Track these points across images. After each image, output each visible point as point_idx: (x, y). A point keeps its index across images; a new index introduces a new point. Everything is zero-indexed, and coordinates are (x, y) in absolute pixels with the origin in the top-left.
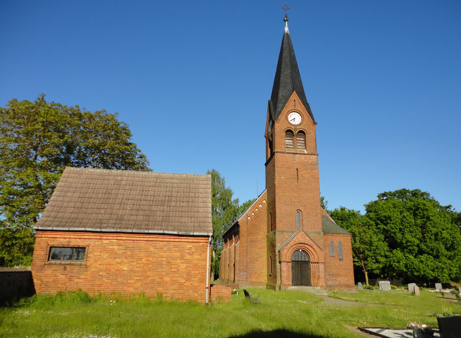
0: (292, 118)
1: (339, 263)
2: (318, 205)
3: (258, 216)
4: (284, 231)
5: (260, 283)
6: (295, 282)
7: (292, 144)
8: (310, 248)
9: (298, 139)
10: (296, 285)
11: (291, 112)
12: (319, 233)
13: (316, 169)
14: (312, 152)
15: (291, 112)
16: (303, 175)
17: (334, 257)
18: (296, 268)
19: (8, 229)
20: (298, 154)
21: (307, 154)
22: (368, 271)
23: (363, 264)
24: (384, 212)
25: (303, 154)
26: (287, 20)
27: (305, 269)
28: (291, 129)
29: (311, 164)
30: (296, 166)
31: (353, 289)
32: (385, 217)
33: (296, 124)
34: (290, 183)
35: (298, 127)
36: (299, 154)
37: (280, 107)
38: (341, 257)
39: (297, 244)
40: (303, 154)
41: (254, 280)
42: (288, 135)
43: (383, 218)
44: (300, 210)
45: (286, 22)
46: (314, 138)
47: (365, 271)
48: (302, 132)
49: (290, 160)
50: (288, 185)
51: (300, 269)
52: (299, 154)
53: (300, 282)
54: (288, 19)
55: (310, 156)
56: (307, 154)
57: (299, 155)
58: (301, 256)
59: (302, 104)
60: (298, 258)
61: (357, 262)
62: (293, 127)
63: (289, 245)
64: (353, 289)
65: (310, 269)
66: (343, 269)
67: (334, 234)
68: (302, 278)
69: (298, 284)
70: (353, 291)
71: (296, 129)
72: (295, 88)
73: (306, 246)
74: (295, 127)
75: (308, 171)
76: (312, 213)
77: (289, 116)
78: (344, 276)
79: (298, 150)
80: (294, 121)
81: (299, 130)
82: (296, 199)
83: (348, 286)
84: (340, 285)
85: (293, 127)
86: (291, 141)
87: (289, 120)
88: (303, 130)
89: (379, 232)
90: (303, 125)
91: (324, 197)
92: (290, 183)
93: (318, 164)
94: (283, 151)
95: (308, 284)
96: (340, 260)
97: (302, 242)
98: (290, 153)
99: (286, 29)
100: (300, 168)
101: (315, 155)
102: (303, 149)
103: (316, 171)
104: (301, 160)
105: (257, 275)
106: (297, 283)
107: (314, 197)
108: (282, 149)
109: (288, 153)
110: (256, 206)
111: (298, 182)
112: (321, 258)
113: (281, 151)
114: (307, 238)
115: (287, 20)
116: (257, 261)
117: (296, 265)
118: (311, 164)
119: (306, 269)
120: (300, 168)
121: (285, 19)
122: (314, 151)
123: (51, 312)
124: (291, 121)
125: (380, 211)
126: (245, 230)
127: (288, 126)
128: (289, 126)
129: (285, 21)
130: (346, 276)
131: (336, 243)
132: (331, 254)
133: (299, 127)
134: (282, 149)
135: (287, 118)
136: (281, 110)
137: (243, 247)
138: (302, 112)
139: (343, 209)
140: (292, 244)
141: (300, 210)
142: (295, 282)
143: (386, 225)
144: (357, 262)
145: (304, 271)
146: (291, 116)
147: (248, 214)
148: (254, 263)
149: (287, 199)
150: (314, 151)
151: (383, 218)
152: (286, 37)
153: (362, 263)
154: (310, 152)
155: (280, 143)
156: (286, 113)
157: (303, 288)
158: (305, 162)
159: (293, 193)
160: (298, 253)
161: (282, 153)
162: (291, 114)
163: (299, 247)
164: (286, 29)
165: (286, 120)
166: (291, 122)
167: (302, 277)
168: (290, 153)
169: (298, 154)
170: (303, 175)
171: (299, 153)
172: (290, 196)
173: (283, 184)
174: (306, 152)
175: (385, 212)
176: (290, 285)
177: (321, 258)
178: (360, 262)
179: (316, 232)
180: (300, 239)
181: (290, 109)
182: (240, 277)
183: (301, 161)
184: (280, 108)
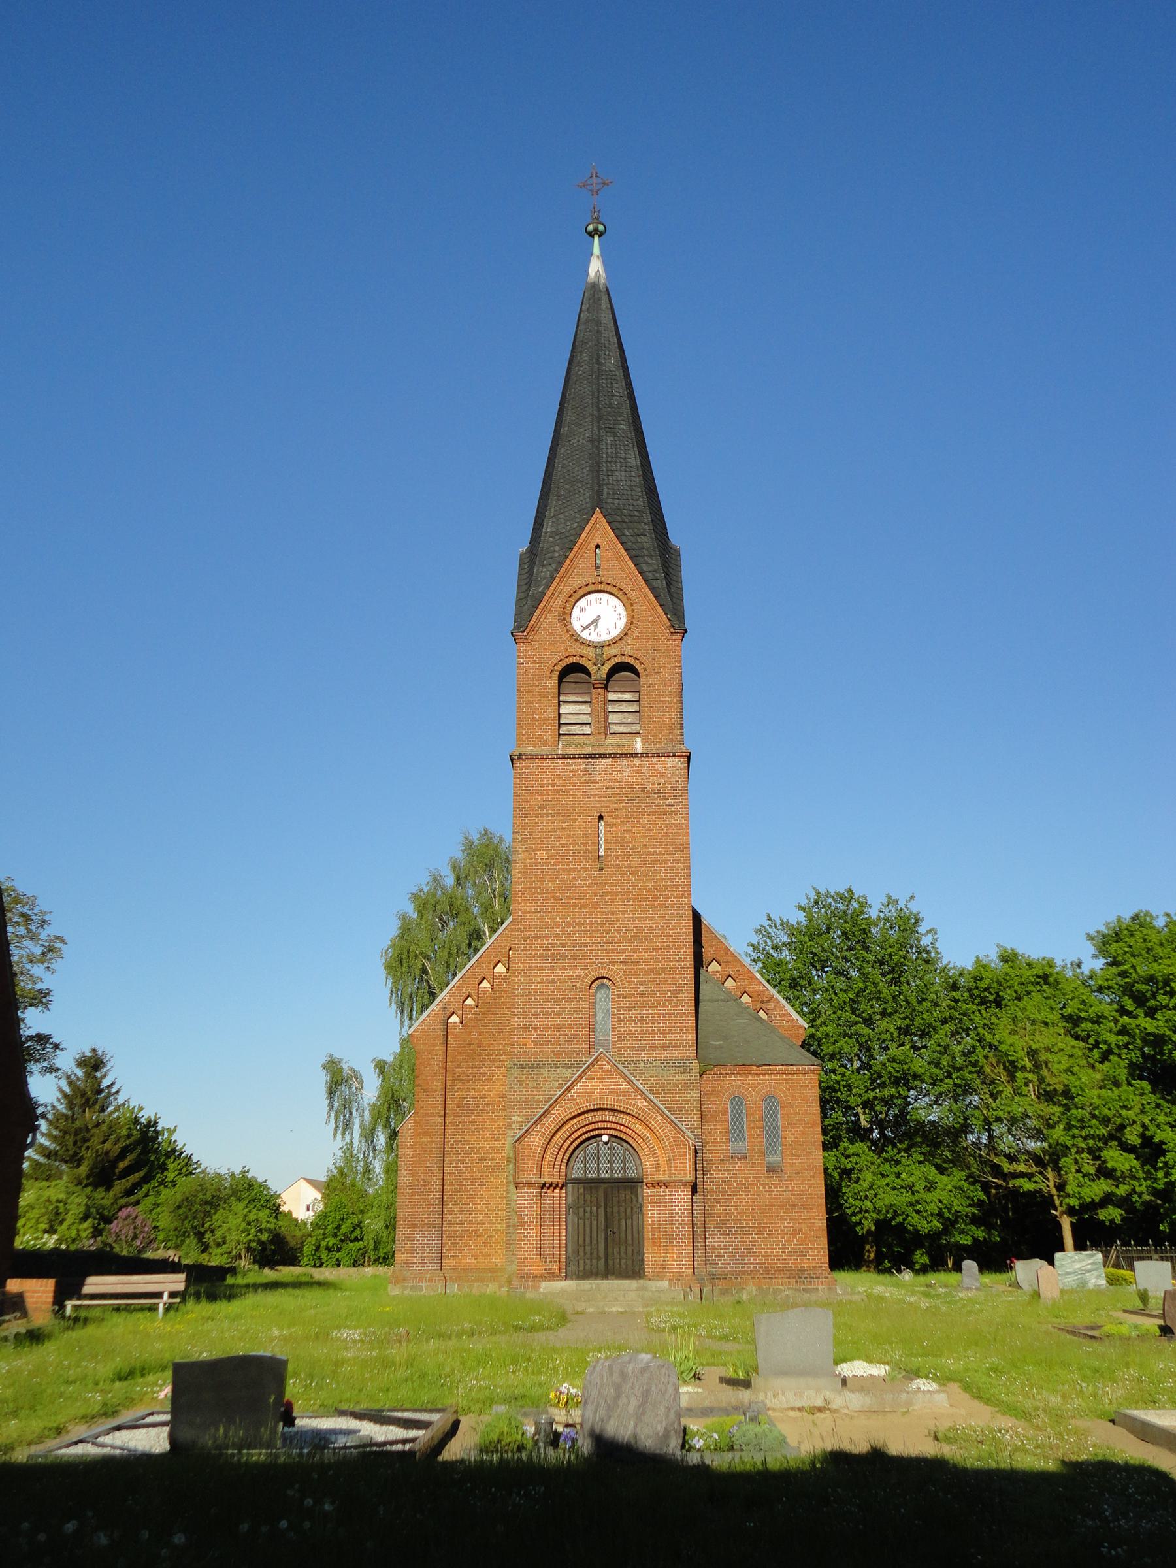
0: (587, 619)
1: (766, 1181)
2: (682, 955)
3: (489, 1010)
4: (541, 1065)
5: (492, 1271)
6: (581, 1262)
7: (587, 719)
8: (639, 1128)
9: (612, 696)
10: (586, 1275)
11: (581, 592)
12: (682, 1065)
13: (676, 812)
14: (664, 744)
15: (581, 592)
16: (623, 838)
17: (744, 1158)
18: (588, 1209)
19: (838, 1097)
20: (605, 756)
21: (641, 756)
22: (1071, 1211)
23: (1051, 1184)
24: (1151, 959)
25: (626, 756)
26: (596, 230)
27: (622, 1209)
28: (582, 661)
29: (658, 793)
30: (598, 806)
31: (820, 1287)
32: (1151, 979)
33: (605, 637)
34: (569, 873)
35: (607, 652)
36: (610, 756)
37: (545, 578)
38: (773, 1159)
39: (587, 1112)
40: (626, 756)
41: (467, 1259)
42: (573, 685)
43: (1144, 987)
44: (607, 978)
45: (596, 237)
46: (674, 687)
47: (1062, 1213)
48: (622, 669)
49: (574, 784)
50: (564, 882)
51: (602, 1210)
52: (610, 756)
53: (603, 1261)
54: (601, 228)
55: (654, 760)
56: (641, 756)
57: (609, 761)
58: (611, 1162)
59: (627, 557)
60: (598, 1168)
61: (1030, 1176)
62: (590, 653)
63: (550, 1118)
64: (820, 1287)
65: (640, 1209)
66: (782, 1205)
67: (749, 1068)
68: (610, 1250)
69: (594, 1271)
70: (821, 1294)
71: (599, 661)
72: (605, 496)
73: (624, 1119)
74: (599, 651)
75: (644, 821)
76: (658, 986)
77: (576, 612)
78: (784, 1234)
79: (611, 740)
80: (596, 627)
81: (614, 661)
82: (591, 937)
83: (799, 1275)
84: (767, 1272)
85: (590, 653)
86: (586, 708)
87: (578, 628)
88: (631, 661)
89: (1126, 1046)
90: (630, 640)
91: (919, 913)
92: (569, 873)
93: (685, 789)
94: (546, 750)
95: (635, 1270)
96: (771, 1169)
97: (602, 1103)
98: (573, 757)
99: (596, 267)
100: (611, 813)
101: (674, 756)
102: (628, 737)
103: (680, 818)
104: (616, 781)
105: (480, 1242)
106: (588, 1267)
107: (667, 924)
108: (545, 744)
109: (564, 757)
110: (484, 970)
111: (601, 869)
112: (680, 1167)
113: (538, 751)
114: (625, 1087)
115: (596, 230)
116: (482, 1184)
117: (588, 1197)
118: (658, 793)
119: (629, 1210)
120: (611, 813)
121: (590, 228)
122: (671, 740)
123: (1106, 1510)
124: (585, 628)
125: (1134, 956)
126: (436, 1067)
127: (571, 651)
128: (575, 648)
129: (591, 235)
130: (795, 1234)
131: (753, 1102)
132: (735, 1147)
133: (613, 651)
134: (545, 744)
135: (565, 619)
136: (544, 588)
137: (426, 1133)
138: (628, 590)
139: (1008, 958)
140: (565, 1116)
141: (607, 978)
142: (581, 1262)
143: (1151, 1013)
144: (1030, 1176)
145: (619, 1220)
146: (583, 610)
147: (448, 1003)
148: (471, 1197)
149: (558, 936)
150: (671, 740)
151: (1144, 987)
152: (596, 296)
153: (1048, 1179)
154: (656, 746)
155: (534, 720)
156: (561, 598)
157: (598, 1284)
158: (632, 788)
159: (579, 913)
160: (598, 1145)
161: (543, 757)
162: (582, 603)
163: (596, 1126)
164: (596, 267)
165: (561, 629)
166: (585, 635)
167: (610, 1244)
168: (573, 757)
169: (605, 756)
170: (623, 838)
171: (607, 752)
172: (569, 925)
173: (542, 880)
174: (639, 746)
175: (1156, 961)
176: (552, 1276)
177: (680, 1167)
178: (1038, 1178)
179: (665, 1064)
180: (597, 1094)
181: (576, 585)
182: (411, 1252)
183: (616, 785)
184: (544, 582)
